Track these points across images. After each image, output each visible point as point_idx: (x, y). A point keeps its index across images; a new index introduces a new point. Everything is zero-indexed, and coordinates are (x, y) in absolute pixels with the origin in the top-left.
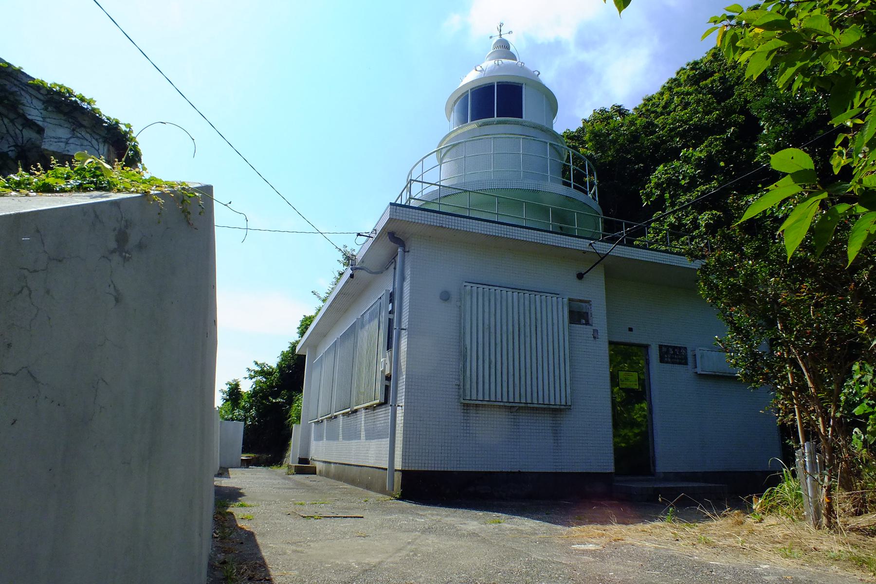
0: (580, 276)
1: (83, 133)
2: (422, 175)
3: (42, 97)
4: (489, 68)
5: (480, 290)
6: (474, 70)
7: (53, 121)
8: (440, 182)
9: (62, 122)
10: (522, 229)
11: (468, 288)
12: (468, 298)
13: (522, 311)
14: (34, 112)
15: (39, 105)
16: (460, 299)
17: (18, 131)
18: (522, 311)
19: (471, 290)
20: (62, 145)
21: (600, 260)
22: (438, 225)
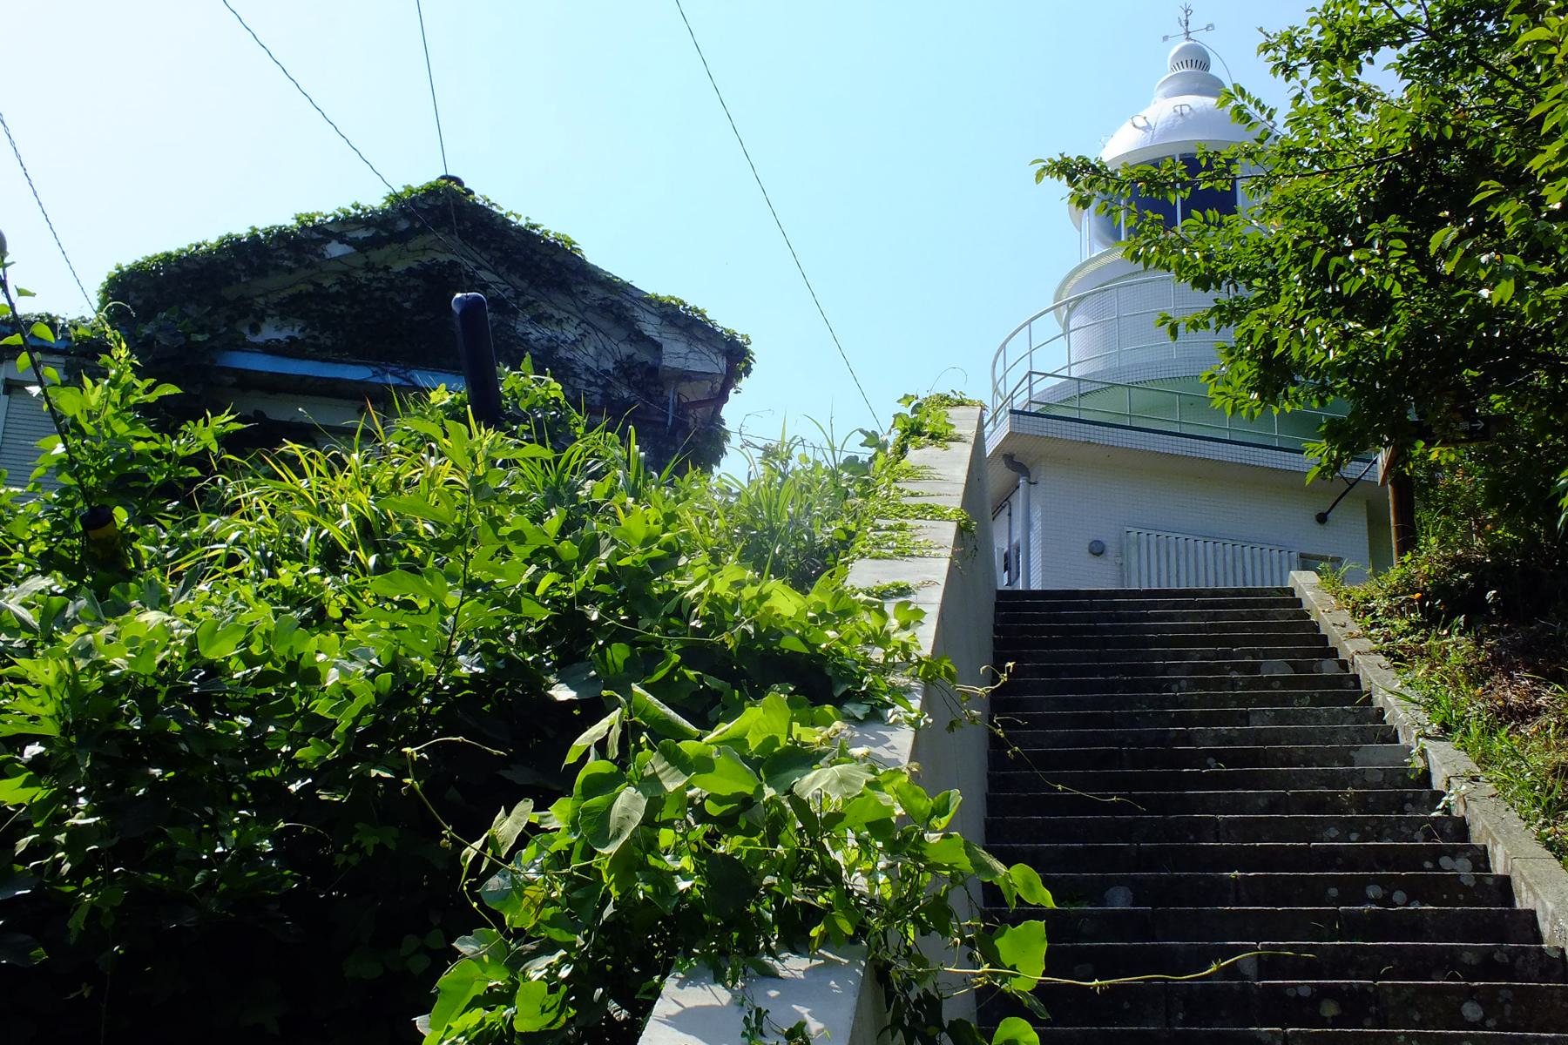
0: (1322, 519)
1: (700, 347)
2: (1030, 353)
3: (653, 310)
4: (1162, 123)
5: (1153, 538)
6: (1128, 125)
7: (669, 336)
8: (1069, 366)
9: (678, 337)
10: (1202, 442)
11: (1134, 534)
12: (1134, 549)
13: (1221, 572)
14: (650, 326)
15: (656, 320)
16: (1121, 553)
17: (615, 347)
18: (1221, 572)
19: (1138, 538)
20: (682, 360)
21: (1350, 488)
22: (1083, 440)
